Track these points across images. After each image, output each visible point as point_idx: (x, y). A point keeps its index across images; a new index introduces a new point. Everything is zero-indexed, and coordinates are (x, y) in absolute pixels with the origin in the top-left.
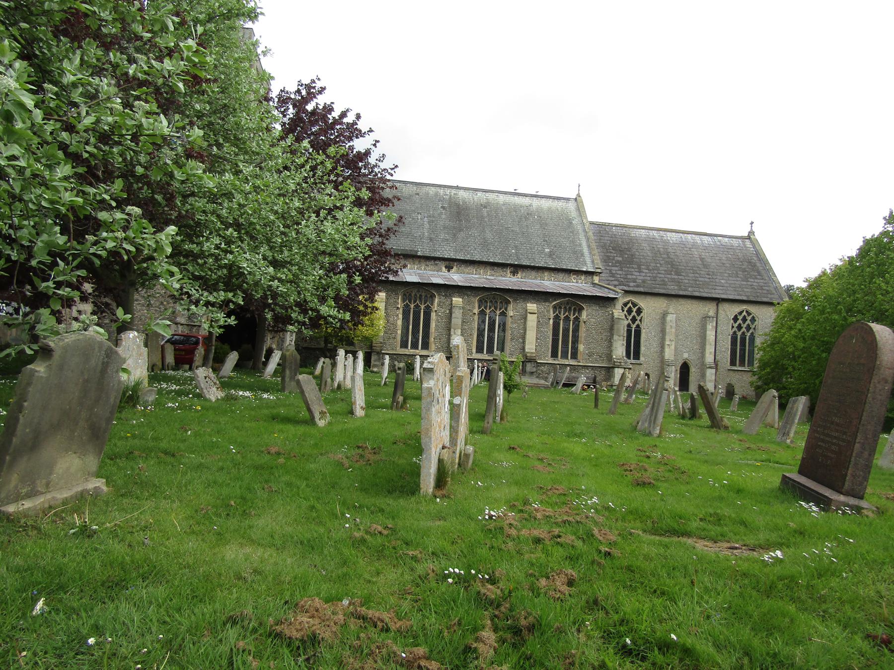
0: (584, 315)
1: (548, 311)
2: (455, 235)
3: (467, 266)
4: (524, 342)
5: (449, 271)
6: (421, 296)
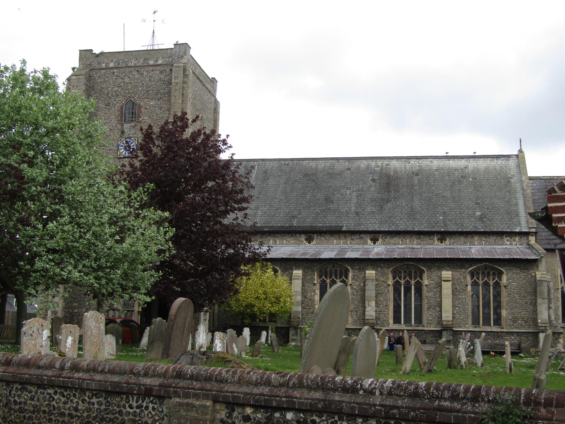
0: (504, 279)
1: (465, 278)
2: (381, 207)
3: (392, 237)
4: (441, 311)
5: (374, 243)
6: (336, 271)
